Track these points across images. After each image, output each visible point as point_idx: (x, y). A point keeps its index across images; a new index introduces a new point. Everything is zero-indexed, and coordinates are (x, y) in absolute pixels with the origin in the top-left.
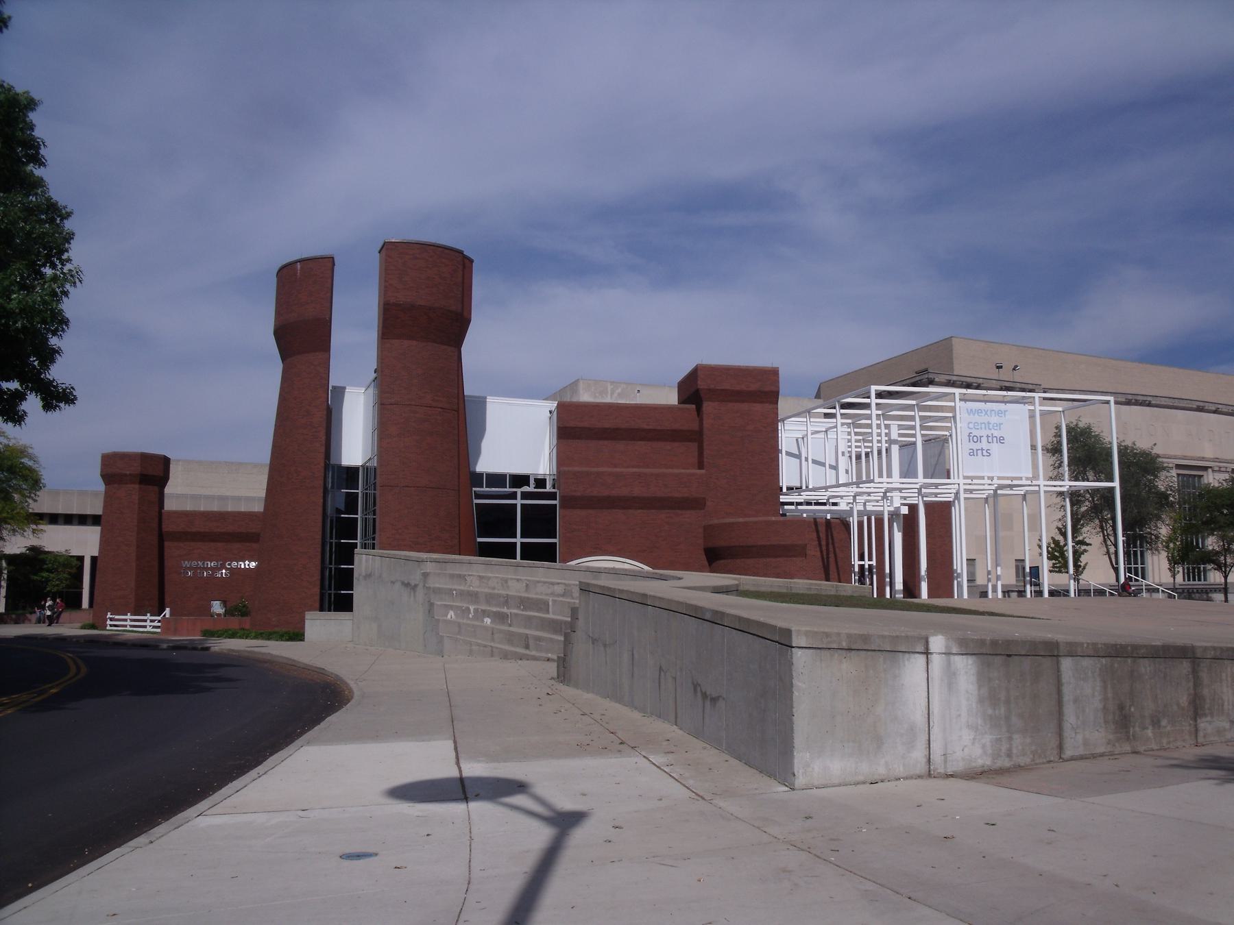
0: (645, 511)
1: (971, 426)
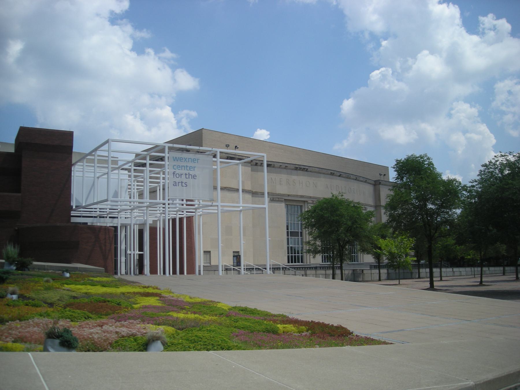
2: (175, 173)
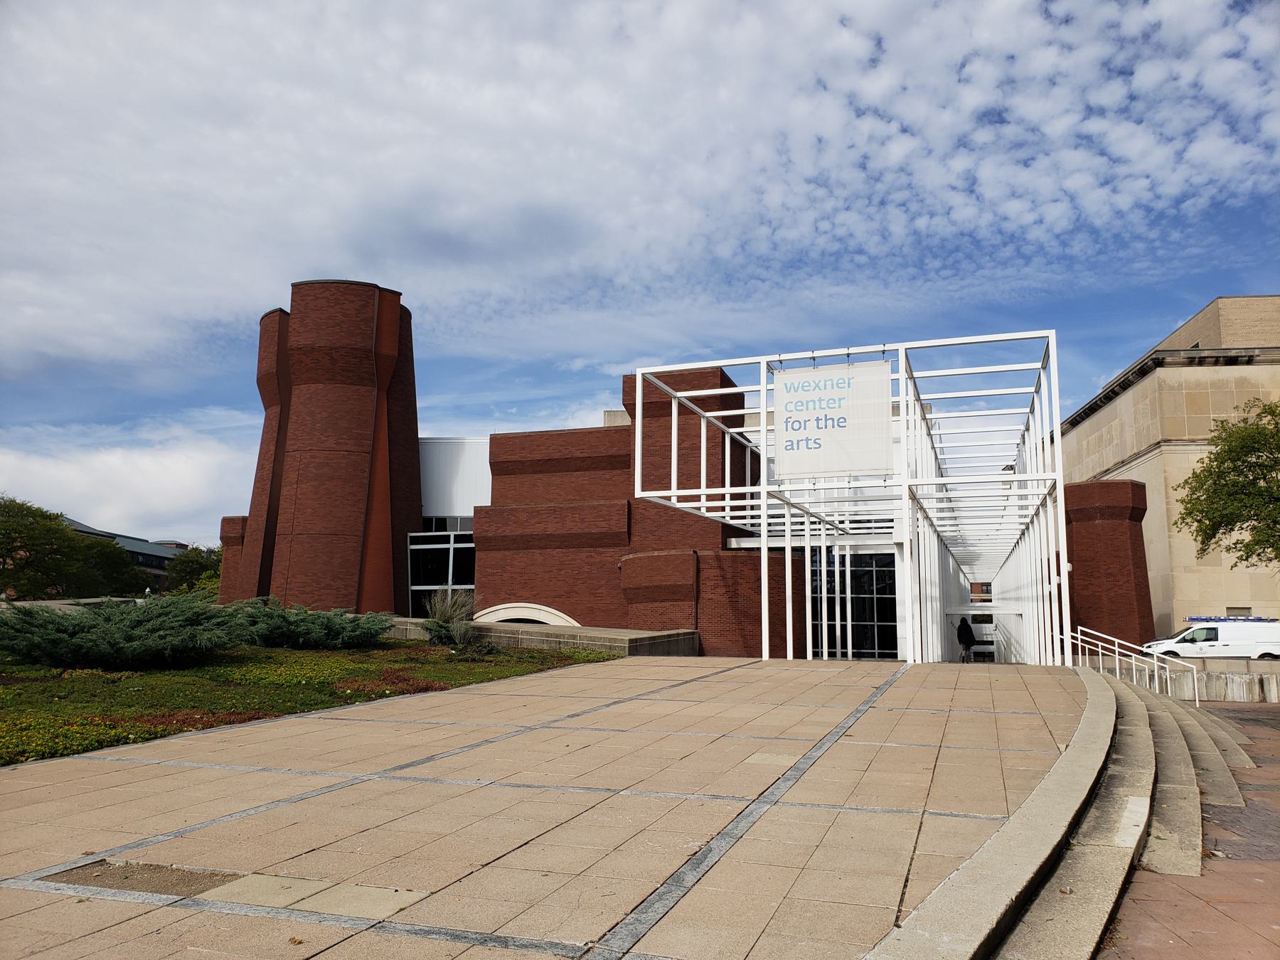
0: (564, 550)
1: (791, 407)
2: (789, 420)
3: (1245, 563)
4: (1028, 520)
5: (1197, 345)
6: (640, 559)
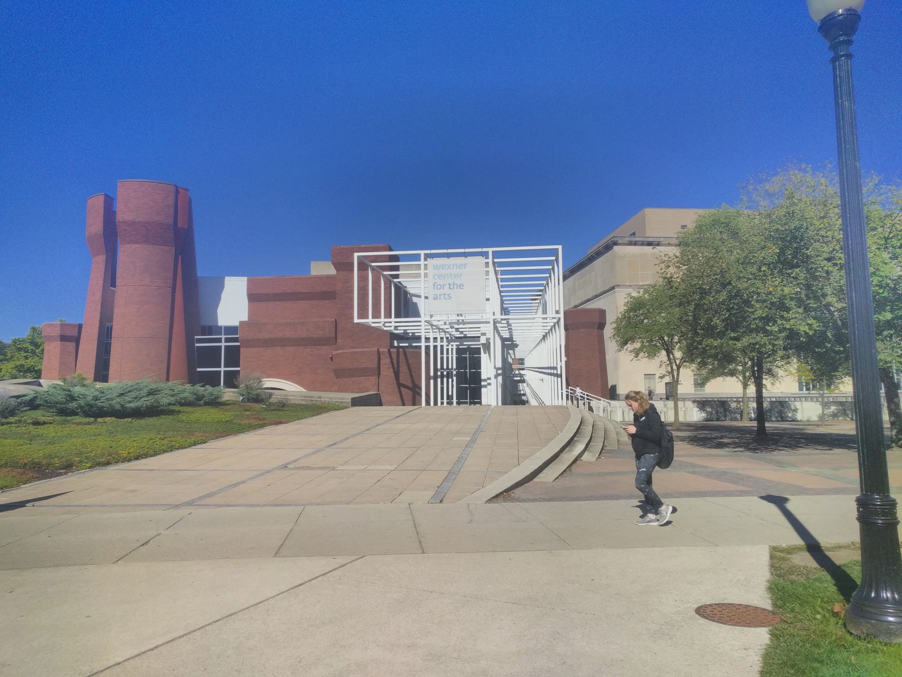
0: (296, 347)
3: (636, 359)
4: (547, 331)
5: (634, 234)
6: (346, 353)
